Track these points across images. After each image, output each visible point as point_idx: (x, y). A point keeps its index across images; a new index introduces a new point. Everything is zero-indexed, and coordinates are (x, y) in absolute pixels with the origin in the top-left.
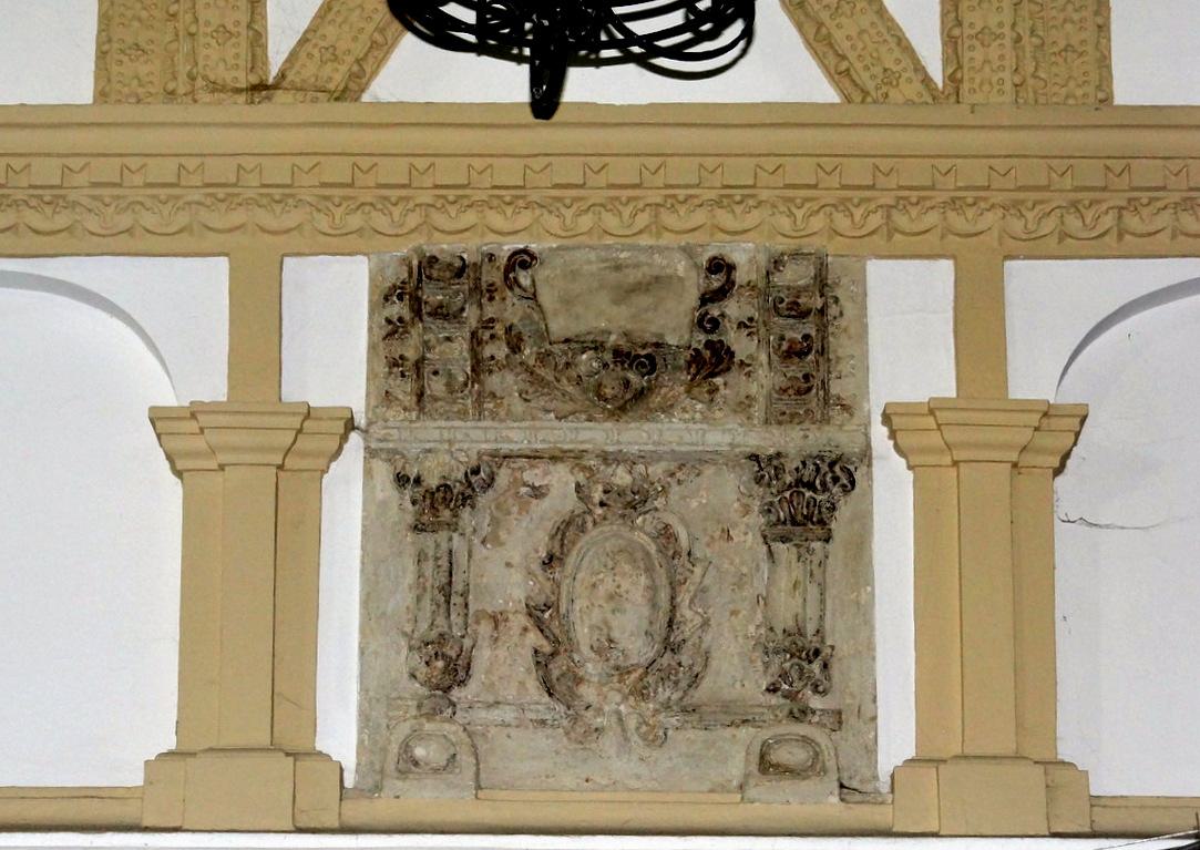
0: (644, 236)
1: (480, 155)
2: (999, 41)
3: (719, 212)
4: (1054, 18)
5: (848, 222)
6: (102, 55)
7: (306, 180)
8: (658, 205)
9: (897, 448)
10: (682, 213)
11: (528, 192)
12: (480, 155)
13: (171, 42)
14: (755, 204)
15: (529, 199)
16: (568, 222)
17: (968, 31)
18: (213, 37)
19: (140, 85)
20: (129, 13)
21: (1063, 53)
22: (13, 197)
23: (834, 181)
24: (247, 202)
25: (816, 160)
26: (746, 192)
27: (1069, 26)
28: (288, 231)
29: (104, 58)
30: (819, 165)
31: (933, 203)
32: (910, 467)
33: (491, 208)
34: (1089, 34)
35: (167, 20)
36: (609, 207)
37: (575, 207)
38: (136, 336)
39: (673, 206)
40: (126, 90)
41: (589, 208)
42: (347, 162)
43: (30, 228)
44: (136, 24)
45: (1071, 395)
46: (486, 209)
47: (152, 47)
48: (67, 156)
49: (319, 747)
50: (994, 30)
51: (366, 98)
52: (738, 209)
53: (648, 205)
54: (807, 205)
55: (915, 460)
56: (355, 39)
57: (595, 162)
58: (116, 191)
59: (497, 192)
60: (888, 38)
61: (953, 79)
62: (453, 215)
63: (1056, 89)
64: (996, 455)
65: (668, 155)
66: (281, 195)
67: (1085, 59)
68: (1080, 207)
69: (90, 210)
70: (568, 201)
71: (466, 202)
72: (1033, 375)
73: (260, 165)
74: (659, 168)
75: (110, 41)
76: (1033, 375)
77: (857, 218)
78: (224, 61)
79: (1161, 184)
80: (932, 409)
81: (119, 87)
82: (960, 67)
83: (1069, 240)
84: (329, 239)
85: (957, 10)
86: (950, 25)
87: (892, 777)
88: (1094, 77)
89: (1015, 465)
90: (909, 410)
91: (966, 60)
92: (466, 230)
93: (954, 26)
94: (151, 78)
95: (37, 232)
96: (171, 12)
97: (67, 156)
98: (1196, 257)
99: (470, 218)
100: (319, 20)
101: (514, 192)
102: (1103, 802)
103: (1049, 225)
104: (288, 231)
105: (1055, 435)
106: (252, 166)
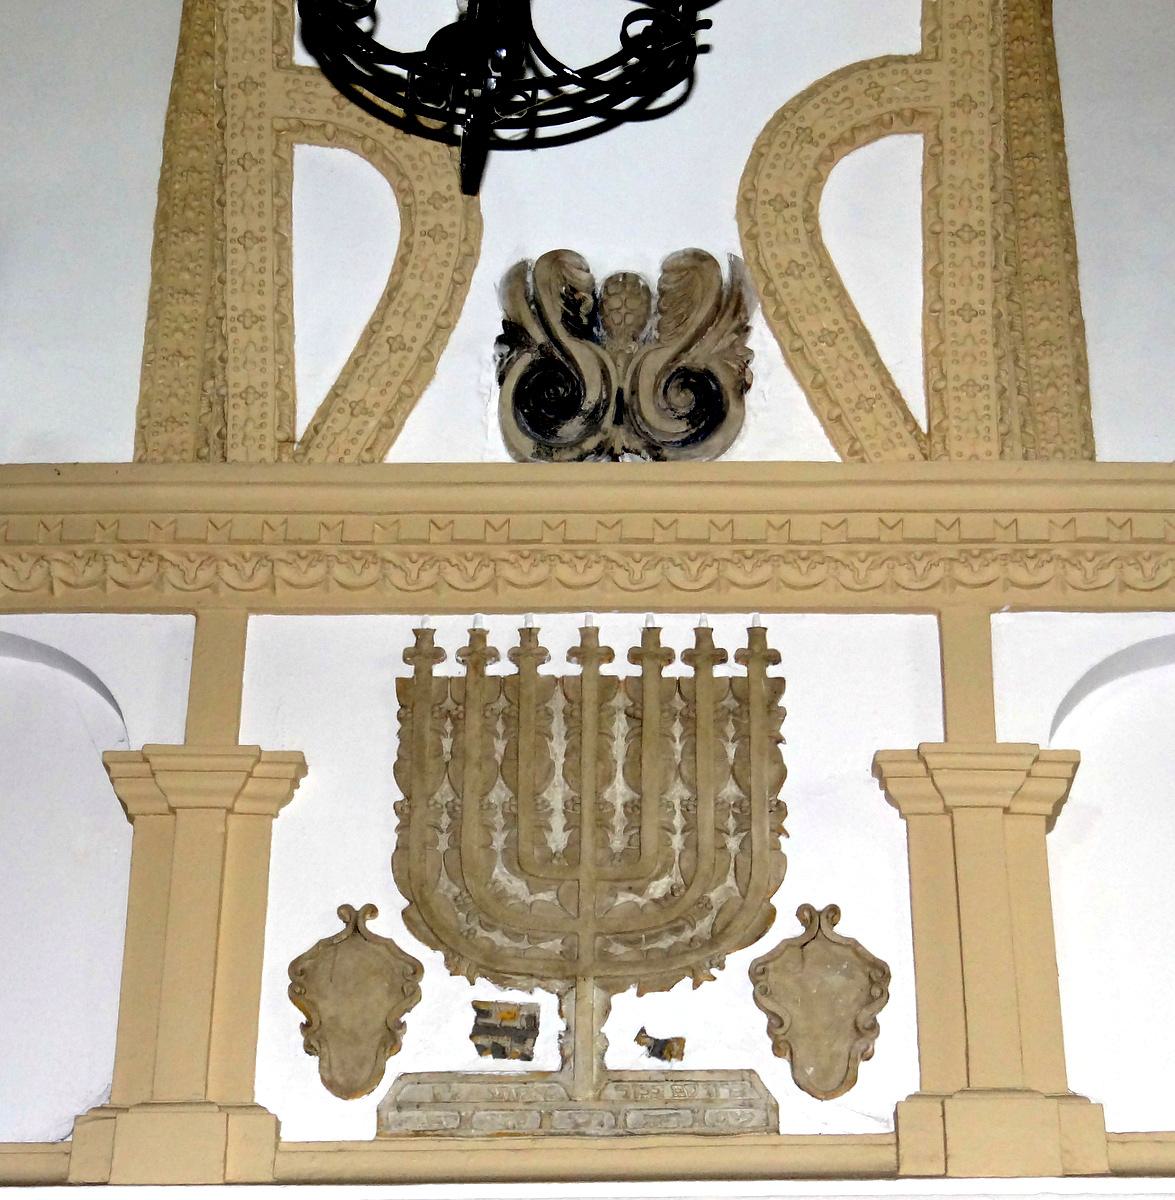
0: (938, 590)
1: (1004, 511)
3: (1011, 566)
5: (1138, 574)
7: (1059, 535)
8: (952, 559)
9: (889, 798)
10: (976, 568)
11: (823, 547)
12: (1004, 511)
14: (820, 560)
15: (1053, 553)
16: (1089, 576)
17: (952, 384)
22: (1053, 553)
23: (726, 535)
24: (548, 558)
25: (877, 515)
26: (759, 547)
27: (173, 400)
28: (590, 585)
30: (432, 522)
31: (995, 554)
32: (902, 816)
33: (563, 562)
36: (678, 561)
37: (1097, 560)
38: (1082, 702)
39: (966, 560)
41: (883, 563)
42: (930, 519)
43: (561, 582)
45: (1061, 742)
46: (781, 563)
48: (603, 512)
49: (259, 1100)
52: (1031, 564)
53: (942, 559)
54: (870, 559)
55: (906, 807)
56: (383, 392)
57: (891, 519)
58: (424, 548)
59: (793, 547)
60: (883, 393)
61: (306, 443)
62: (525, 570)
64: (983, 800)
65: (511, 512)
66: (975, 550)
68: (1140, 558)
69: (621, 566)
70: (862, 556)
71: (1045, 557)
72: (1019, 718)
73: (118, 521)
74: (1125, 524)
76: (1019, 718)
77: (920, 571)
79: (818, 538)
80: (920, 754)
83: (1128, 590)
84: (628, 594)
87: (896, 1114)
89: (1006, 810)
90: (897, 756)
92: (816, 585)
95: (794, 587)
97: (657, 512)
98: (1166, 610)
99: (766, 571)
100: (347, 376)
101: (1036, 546)
102: (1137, 1138)
103: (1107, 576)
104: (590, 585)
105: (1046, 782)
106: (557, 522)
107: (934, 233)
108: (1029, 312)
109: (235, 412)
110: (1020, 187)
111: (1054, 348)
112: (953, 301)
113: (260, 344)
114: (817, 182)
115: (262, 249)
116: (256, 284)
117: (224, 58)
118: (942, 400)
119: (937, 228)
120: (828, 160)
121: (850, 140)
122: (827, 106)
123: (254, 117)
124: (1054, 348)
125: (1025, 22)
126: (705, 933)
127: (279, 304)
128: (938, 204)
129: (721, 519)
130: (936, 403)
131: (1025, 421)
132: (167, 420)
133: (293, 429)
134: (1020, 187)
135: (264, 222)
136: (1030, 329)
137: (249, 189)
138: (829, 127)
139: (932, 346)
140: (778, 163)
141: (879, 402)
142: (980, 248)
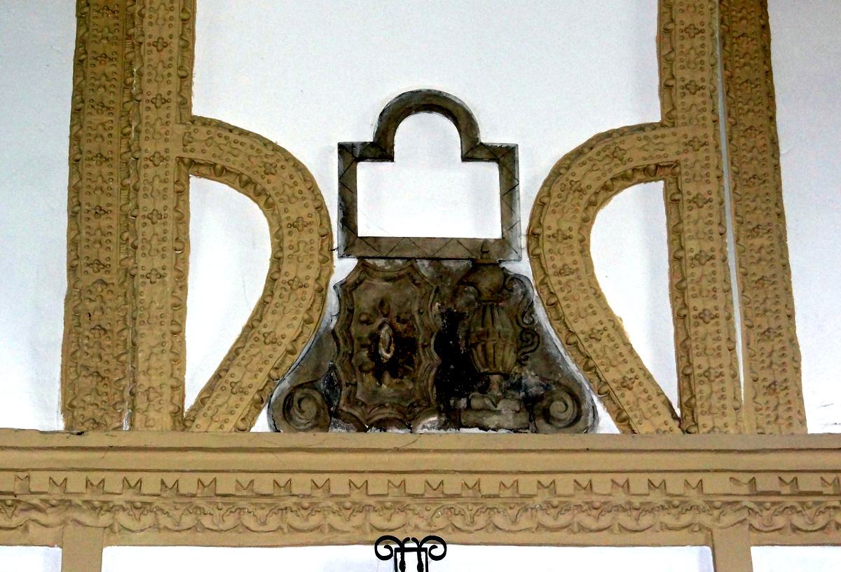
2: (700, 35)
4: (744, 156)
6: (76, 112)
13: (125, 153)
18: (149, 218)
19: (104, 182)
20: (94, 185)
21: (756, 230)
29: (75, 271)
34: (770, 169)
35: (127, 39)
40: (97, 83)
44: (105, 42)
47: (110, 208)
50: (696, 27)
51: (253, 430)
63: (745, 153)
67: (767, 184)
75: (80, 204)
78: (164, 4)
81: (89, 183)
82: (674, 108)
85: (688, 355)
86: (672, 192)
88: (773, 197)
91: (697, 390)
93: (678, 250)
94: (115, 76)
96: (124, 184)
107: (686, 375)
108: (740, 105)
109: (144, 229)
110: (734, 13)
111: (757, 133)
112: (699, 367)
113: (163, 177)
114: (587, 222)
115: (164, 224)
116: (160, 250)
117: (141, 79)
118: (689, 383)
119: (688, 371)
120: (595, 204)
121: (608, 190)
122: (592, 163)
123: (162, 124)
124: (757, 133)
125: (752, 68)
126: (479, 278)
127: (177, 206)
128: (693, 412)
129: (508, 480)
130: (686, 384)
131: (736, 185)
132: (103, 9)
133: (183, 400)
134: (734, 13)
135: (170, 87)
136: (734, 24)
137: (155, 237)
138: (592, 181)
139: (685, 399)
140: (557, 209)
141: (637, 381)
142: (702, 99)
